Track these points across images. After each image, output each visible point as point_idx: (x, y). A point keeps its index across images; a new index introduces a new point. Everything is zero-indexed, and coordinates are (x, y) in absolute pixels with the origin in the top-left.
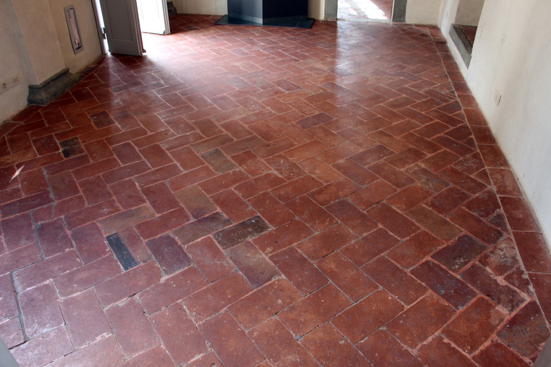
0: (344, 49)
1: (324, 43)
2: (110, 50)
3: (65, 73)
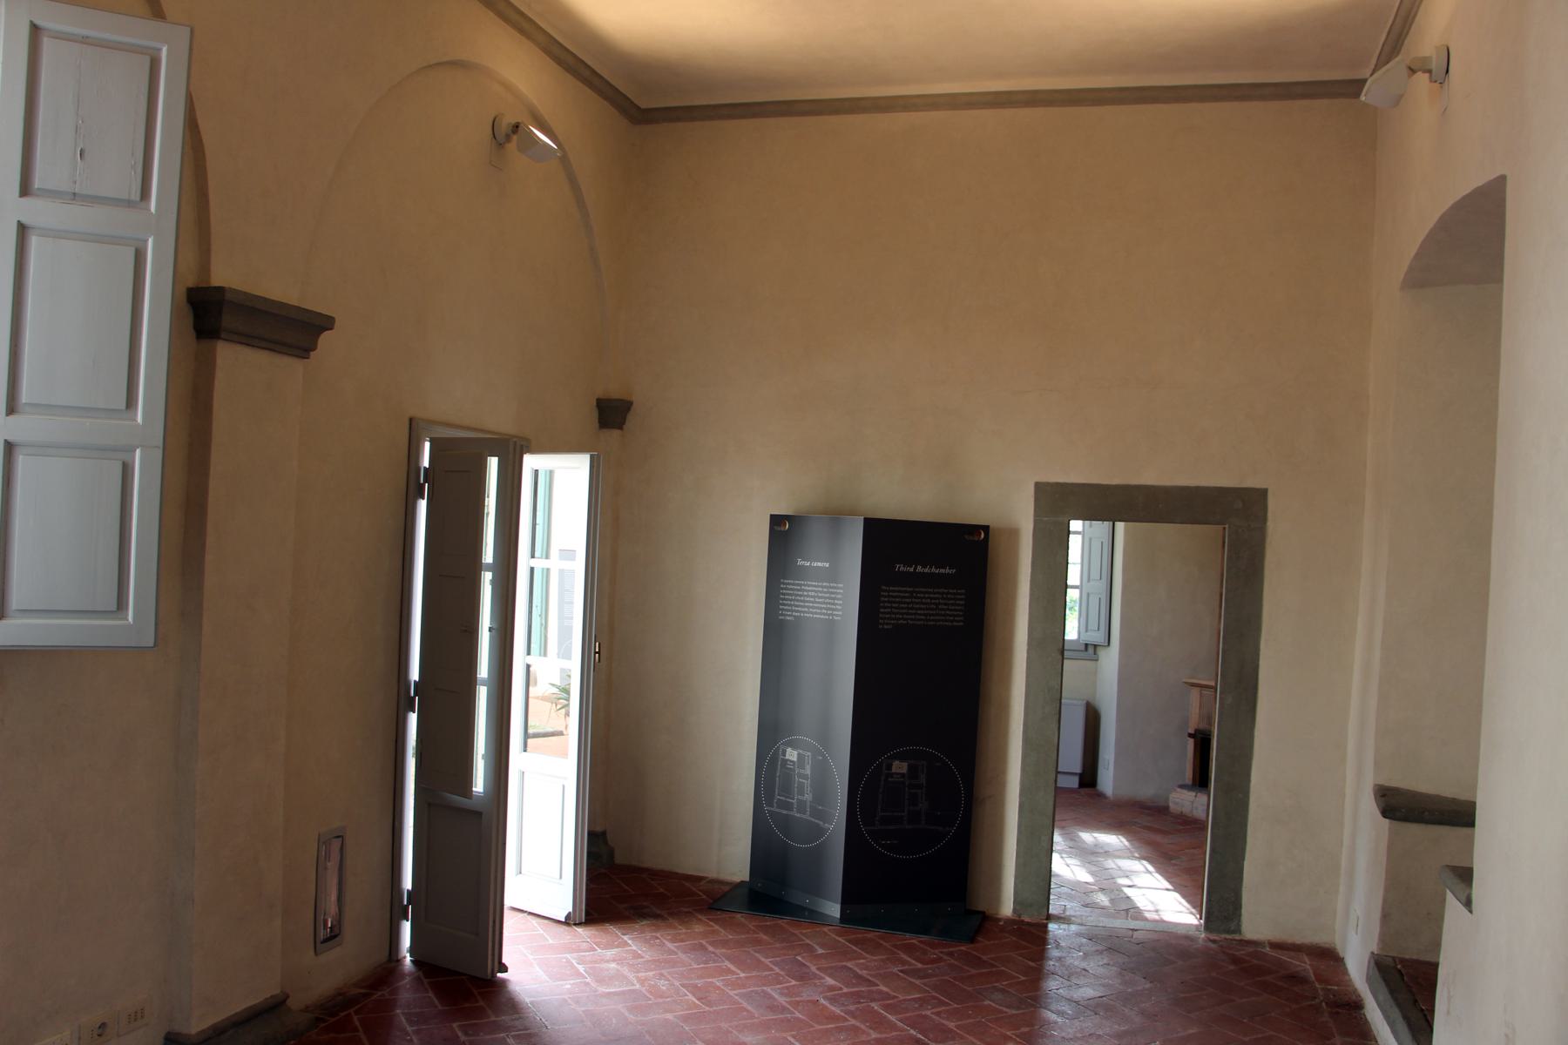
0: (1060, 1013)
1: (1003, 991)
2: (412, 950)
3: (275, 1007)
